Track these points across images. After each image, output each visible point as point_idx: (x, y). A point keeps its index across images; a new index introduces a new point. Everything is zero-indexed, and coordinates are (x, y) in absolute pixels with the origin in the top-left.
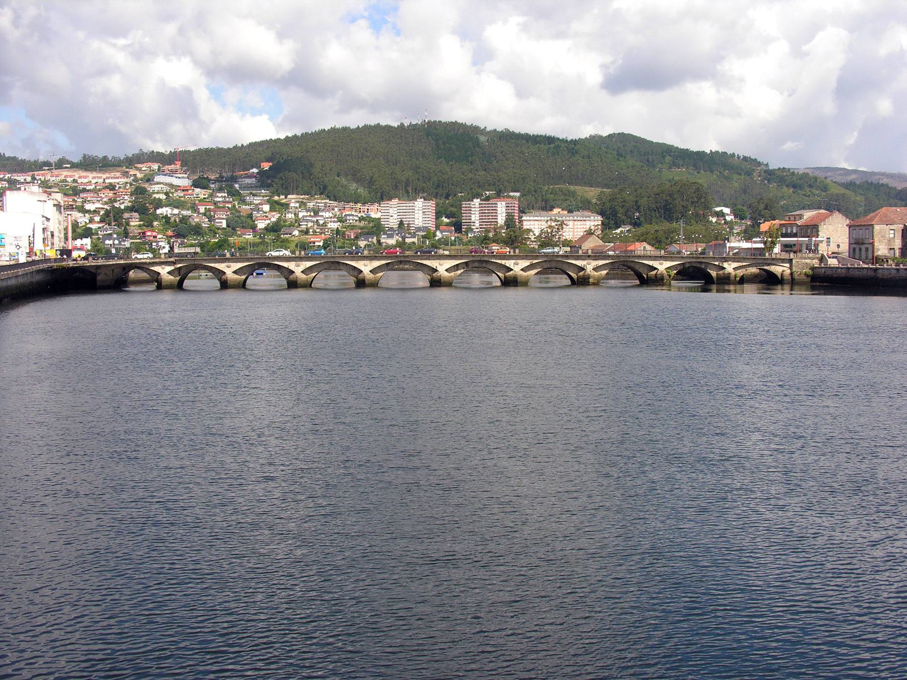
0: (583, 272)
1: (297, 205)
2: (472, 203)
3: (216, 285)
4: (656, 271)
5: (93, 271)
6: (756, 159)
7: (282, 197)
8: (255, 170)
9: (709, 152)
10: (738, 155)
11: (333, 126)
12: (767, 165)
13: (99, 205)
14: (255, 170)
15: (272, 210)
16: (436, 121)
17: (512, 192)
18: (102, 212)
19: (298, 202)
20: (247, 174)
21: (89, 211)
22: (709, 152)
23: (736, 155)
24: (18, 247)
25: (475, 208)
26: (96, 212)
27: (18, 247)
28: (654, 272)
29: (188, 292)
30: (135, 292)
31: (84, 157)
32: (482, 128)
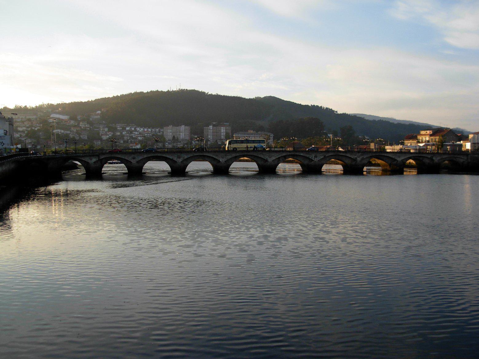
0: (355, 162)
1: (121, 128)
2: (208, 128)
3: (299, 168)
4: (396, 161)
5: (424, 147)
6: (332, 109)
7: (114, 125)
8: (99, 112)
9: (310, 105)
10: (324, 107)
11: (136, 91)
12: (337, 112)
13: (25, 128)
14: (99, 112)
15: (109, 131)
16: (185, 89)
17: (225, 122)
18: (26, 132)
19: (121, 127)
20: (95, 114)
21: (20, 131)
22: (310, 105)
23: (323, 107)
24: (2, 144)
25: (210, 130)
26: (23, 132)
27: (2, 144)
28: (395, 162)
29: (324, 176)
30: (253, 171)
31: (16, 106)
32: (207, 93)
